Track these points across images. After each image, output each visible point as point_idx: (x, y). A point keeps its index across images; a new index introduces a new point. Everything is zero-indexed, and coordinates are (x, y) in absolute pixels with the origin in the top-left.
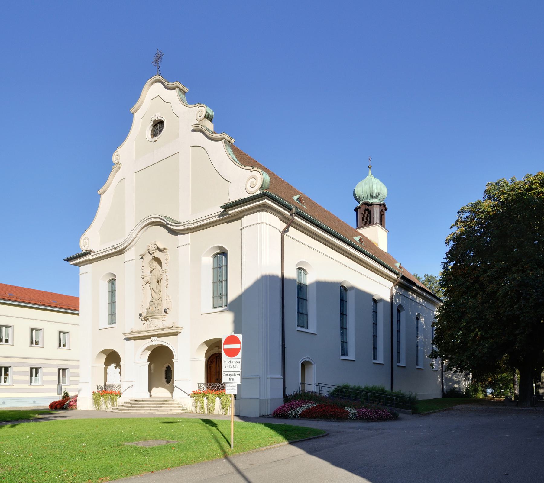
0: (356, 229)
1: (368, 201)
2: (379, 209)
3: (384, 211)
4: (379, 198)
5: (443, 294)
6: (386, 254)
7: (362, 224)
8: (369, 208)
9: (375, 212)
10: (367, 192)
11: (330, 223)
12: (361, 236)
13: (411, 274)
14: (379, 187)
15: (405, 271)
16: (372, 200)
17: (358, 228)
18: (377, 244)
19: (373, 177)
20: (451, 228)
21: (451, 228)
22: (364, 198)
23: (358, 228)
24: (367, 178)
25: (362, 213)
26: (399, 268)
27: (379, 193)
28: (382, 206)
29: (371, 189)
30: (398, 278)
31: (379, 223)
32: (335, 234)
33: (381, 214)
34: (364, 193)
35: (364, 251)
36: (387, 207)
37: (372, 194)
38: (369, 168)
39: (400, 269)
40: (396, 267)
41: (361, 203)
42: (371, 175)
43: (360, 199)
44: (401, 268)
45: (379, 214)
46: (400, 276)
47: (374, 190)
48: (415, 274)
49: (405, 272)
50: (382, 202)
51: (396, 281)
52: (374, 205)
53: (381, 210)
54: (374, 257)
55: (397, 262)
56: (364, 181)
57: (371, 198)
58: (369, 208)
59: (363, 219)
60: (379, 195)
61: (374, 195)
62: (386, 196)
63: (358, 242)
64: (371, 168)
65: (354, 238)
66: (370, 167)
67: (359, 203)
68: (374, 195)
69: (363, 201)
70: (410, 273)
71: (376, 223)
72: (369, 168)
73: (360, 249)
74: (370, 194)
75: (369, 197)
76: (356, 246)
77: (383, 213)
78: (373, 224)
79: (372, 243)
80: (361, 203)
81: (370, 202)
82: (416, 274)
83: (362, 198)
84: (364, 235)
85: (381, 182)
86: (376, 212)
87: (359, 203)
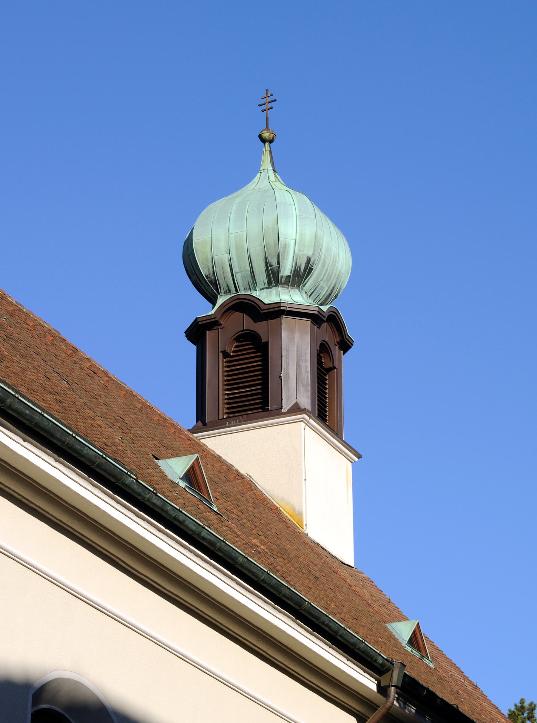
0: (194, 430)
1: (256, 294)
2: (308, 338)
3: (336, 350)
4: (310, 283)
5: (239, 559)
6: (343, 572)
7: (223, 409)
8: (260, 328)
9: (288, 351)
10: (252, 251)
11: (24, 370)
12: (195, 456)
13: (476, 687)
14: (309, 232)
15: (447, 672)
16: (274, 290)
17: (204, 424)
18: (300, 514)
19: (280, 187)
20: (272, 108)
21: (272, 108)
22: (238, 277)
23: (204, 424)
24: (252, 185)
25: (226, 355)
26: (409, 649)
27: (309, 260)
28: (325, 325)
29: (271, 240)
30: (382, 690)
31: (308, 407)
32: (9, 401)
33: (320, 363)
34: (234, 256)
35: (181, 518)
36: (350, 332)
37: (274, 262)
38: (263, 141)
39: (415, 652)
40: (391, 638)
41: (221, 300)
42: (271, 173)
43: (215, 283)
44: (419, 650)
45: (309, 364)
46: (396, 677)
47: (285, 246)
48: (522, 701)
49: (441, 672)
50: (325, 308)
51: (372, 706)
52: (286, 320)
53: (317, 347)
54: (241, 559)
55: (402, 618)
56: (238, 200)
57: (270, 283)
58: (260, 328)
59: (231, 384)
60: (309, 270)
61: (286, 270)
62: (345, 280)
63: (182, 484)
64: (271, 141)
65: (160, 463)
66: (266, 135)
67: (213, 300)
68: (286, 270)
69: (230, 292)
70: (470, 682)
71: (296, 409)
72: (263, 141)
73: (158, 503)
74: (267, 264)
75: (261, 277)
76: (135, 487)
77: (332, 359)
78: (278, 412)
79: (275, 510)
80: (221, 300)
81: (267, 301)
82: (526, 704)
83: (225, 279)
84: (230, 461)
85: (318, 211)
86: (293, 350)
87: (213, 300)
